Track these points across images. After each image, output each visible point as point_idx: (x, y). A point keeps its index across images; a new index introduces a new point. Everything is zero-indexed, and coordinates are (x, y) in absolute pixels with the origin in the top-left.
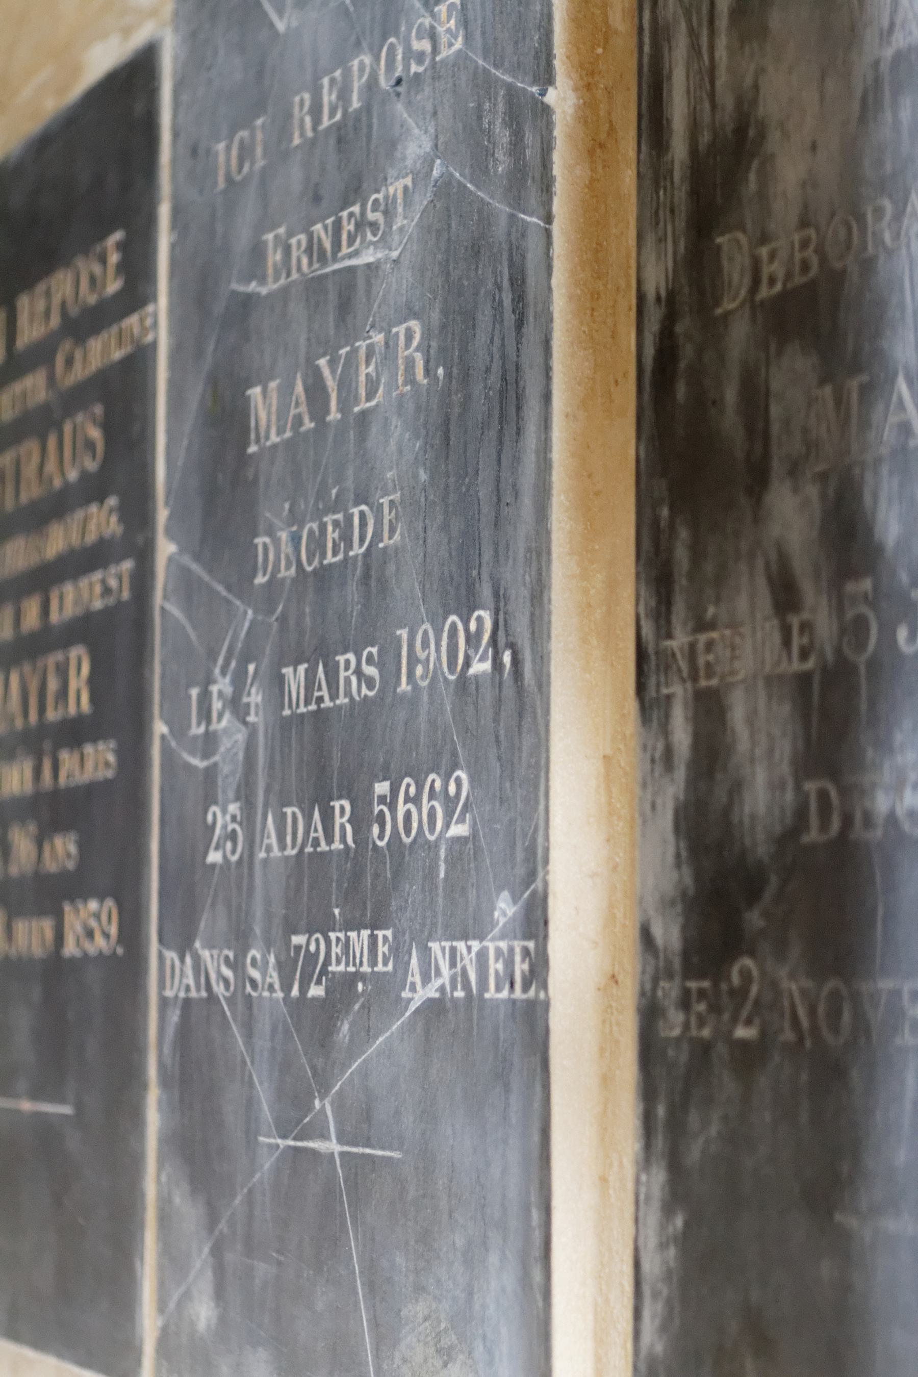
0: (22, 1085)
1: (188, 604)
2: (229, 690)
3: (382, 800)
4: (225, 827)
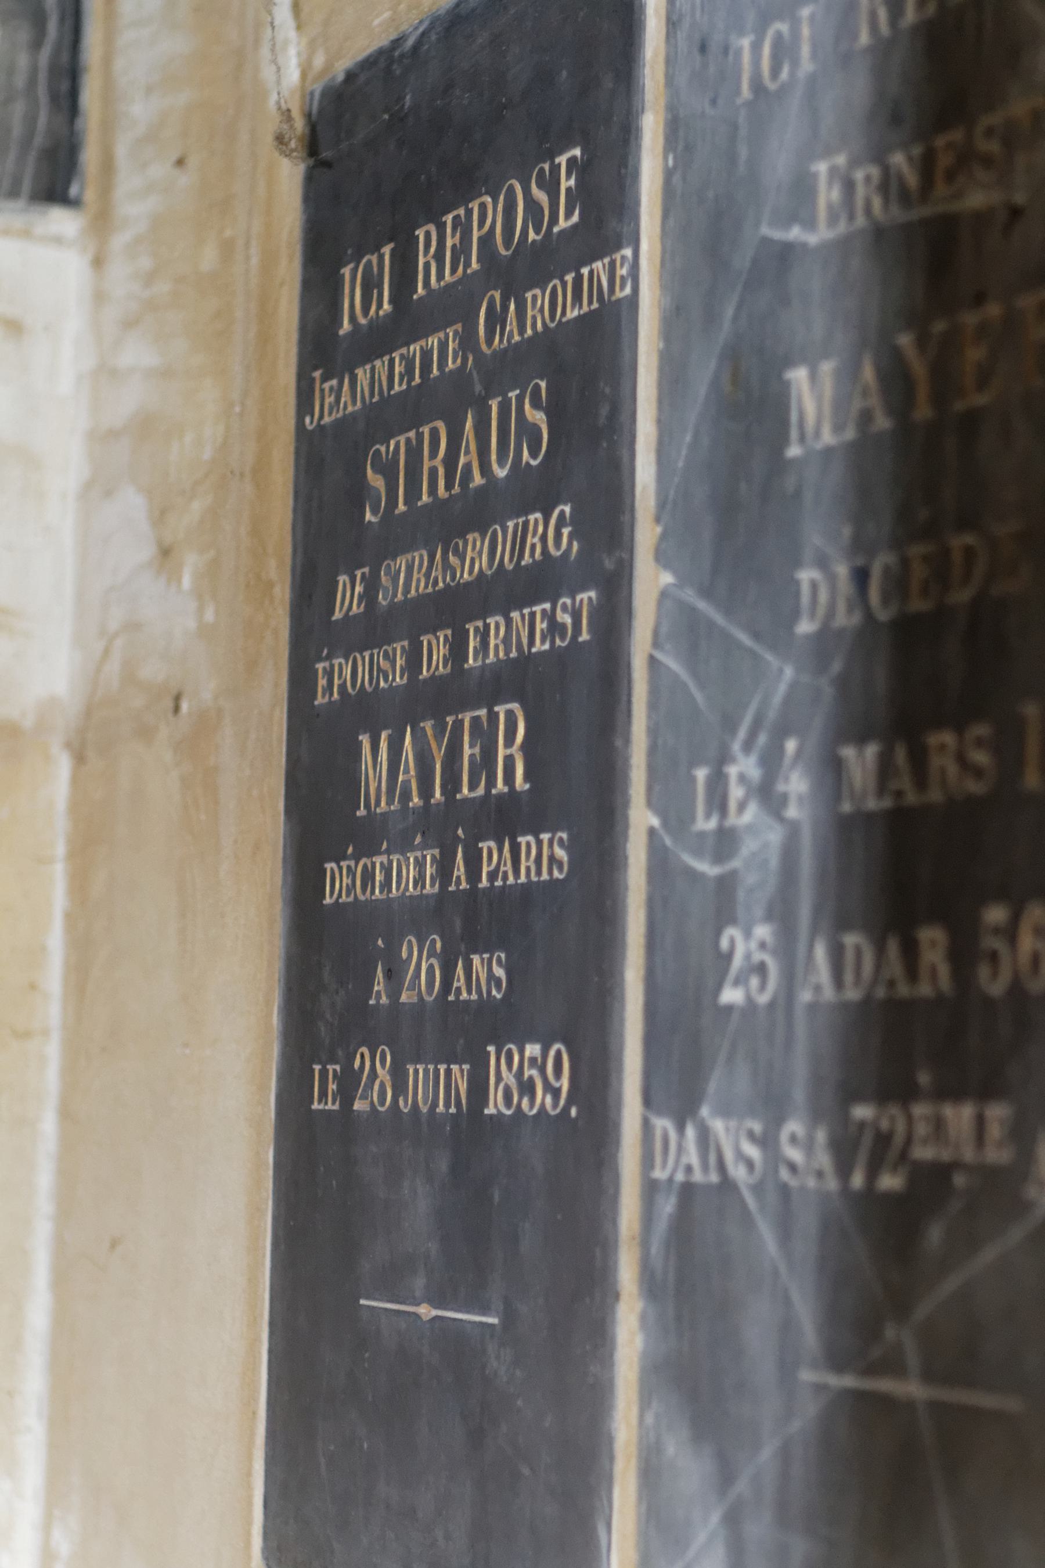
0: (419, 1283)
1: (692, 657)
2: (755, 773)
3: (996, 931)
4: (748, 956)
